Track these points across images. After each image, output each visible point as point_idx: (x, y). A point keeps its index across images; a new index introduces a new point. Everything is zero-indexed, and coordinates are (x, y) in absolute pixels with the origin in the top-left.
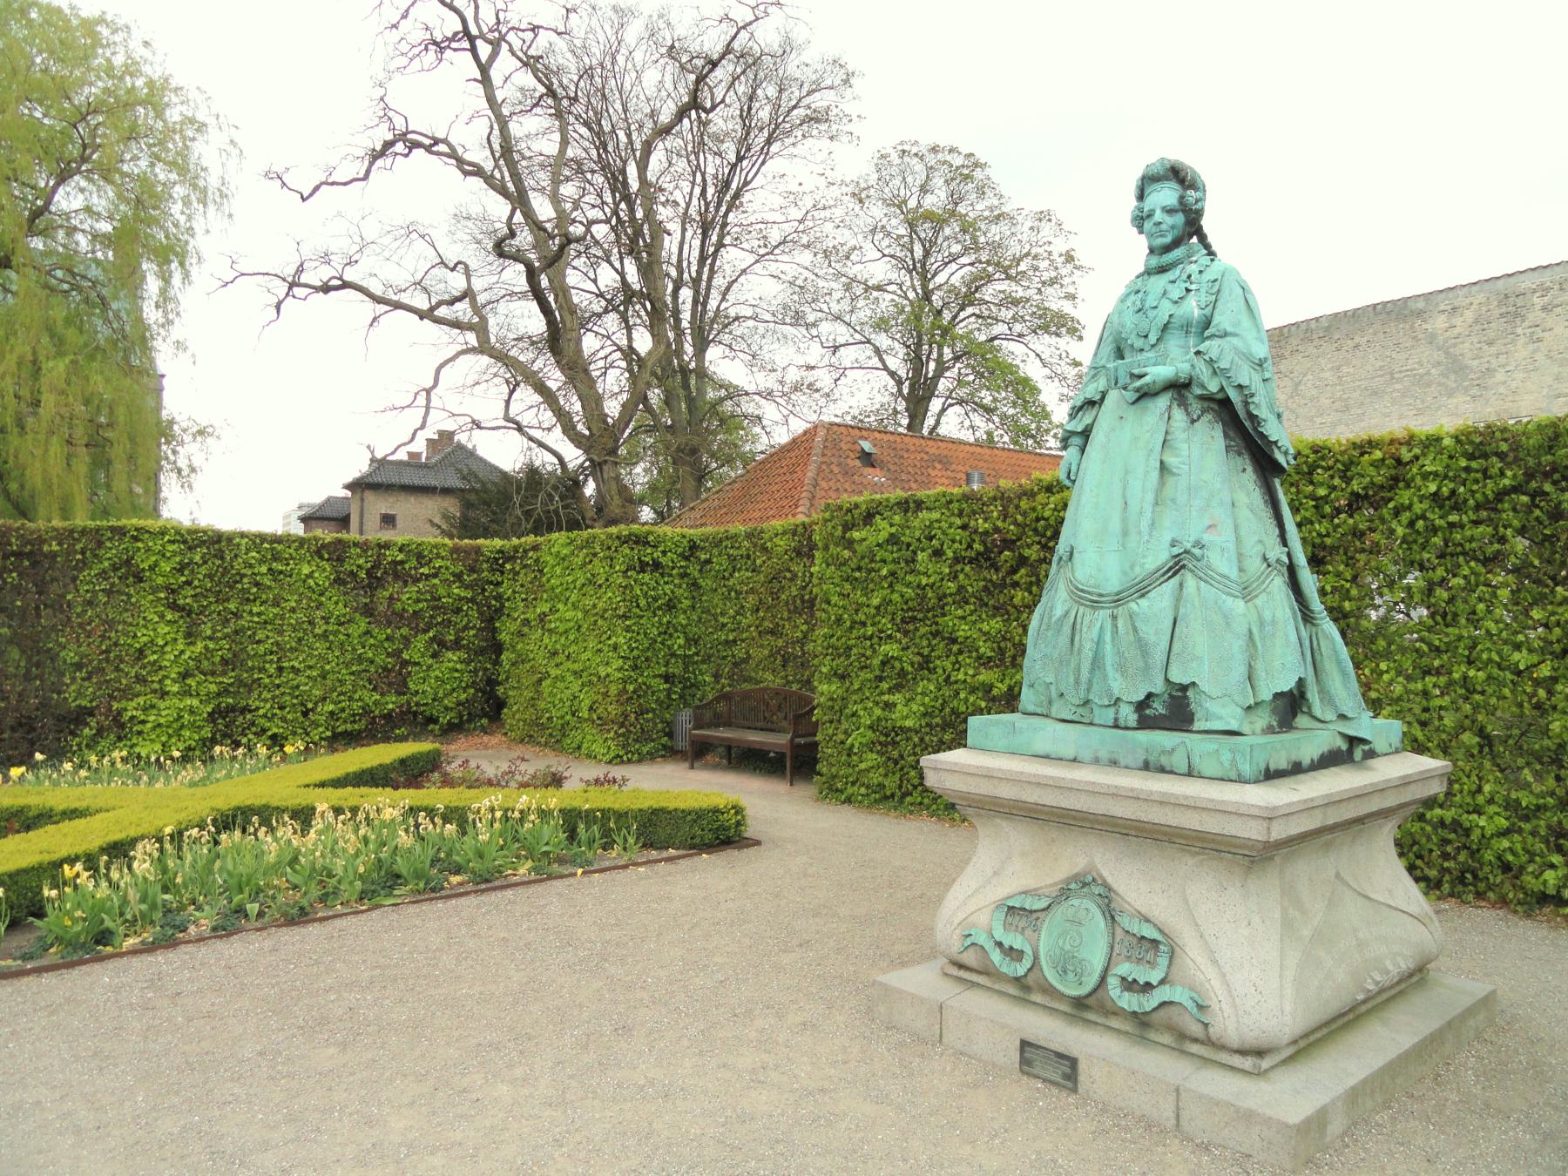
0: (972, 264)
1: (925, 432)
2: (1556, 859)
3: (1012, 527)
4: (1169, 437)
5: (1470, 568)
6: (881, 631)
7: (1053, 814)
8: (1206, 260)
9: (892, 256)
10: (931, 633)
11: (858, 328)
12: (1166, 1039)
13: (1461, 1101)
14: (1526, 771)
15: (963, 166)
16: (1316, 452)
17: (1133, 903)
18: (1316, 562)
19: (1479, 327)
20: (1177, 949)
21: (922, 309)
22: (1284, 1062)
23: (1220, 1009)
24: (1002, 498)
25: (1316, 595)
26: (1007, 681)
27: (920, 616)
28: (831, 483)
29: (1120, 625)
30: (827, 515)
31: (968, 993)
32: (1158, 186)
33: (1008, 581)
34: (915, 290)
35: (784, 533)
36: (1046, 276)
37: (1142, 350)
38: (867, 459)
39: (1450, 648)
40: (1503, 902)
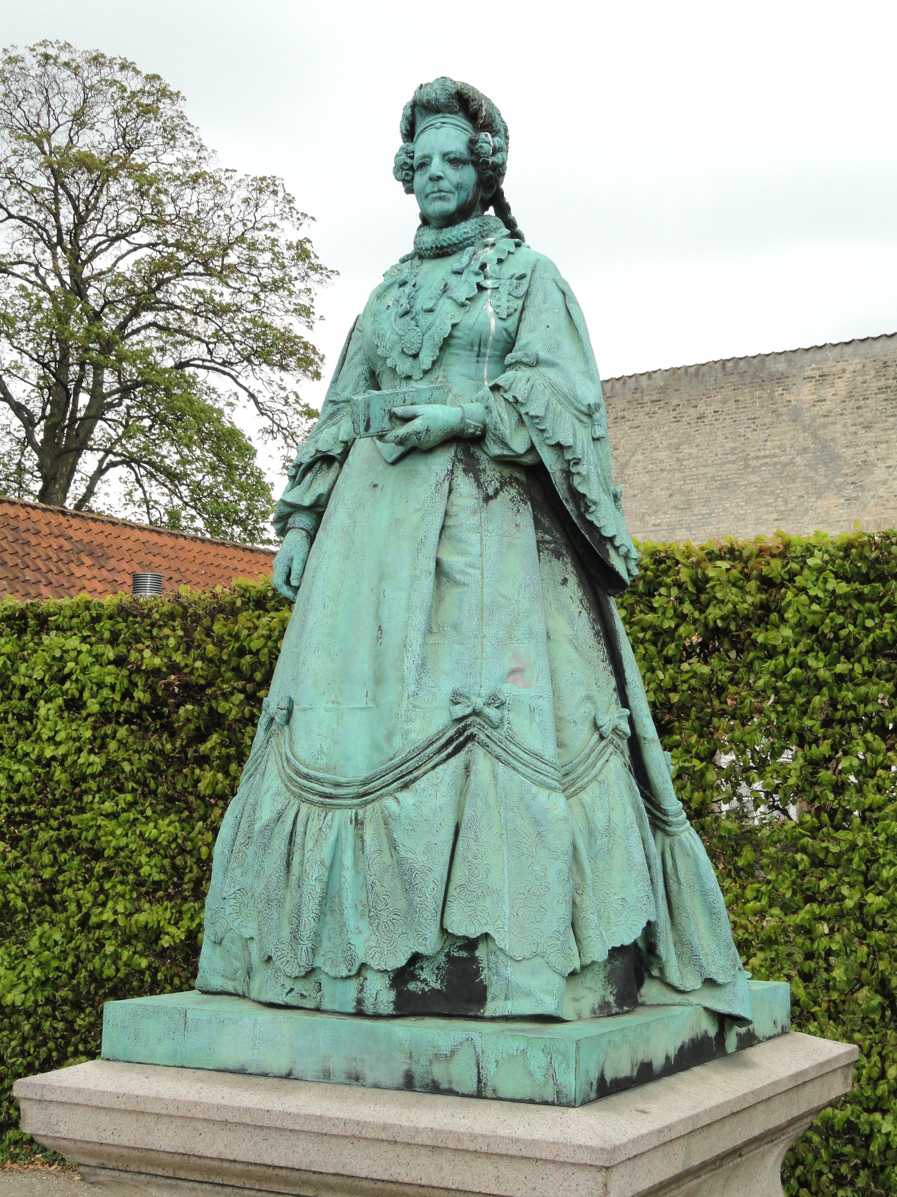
0: (152, 246)
1: (70, 504)
3: (198, 664)
4: (449, 522)
7: (247, 1175)
8: (510, 243)
9: (22, 219)
10: (59, 841)
15: (142, 91)
19: (852, 404)
24: (184, 616)
25: (670, 786)
26: (185, 923)
27: (41, 812)
29: (368, 838)
32: (437, 119)
33: (190, 753)
36: (267, 276)
37: (409, 378)
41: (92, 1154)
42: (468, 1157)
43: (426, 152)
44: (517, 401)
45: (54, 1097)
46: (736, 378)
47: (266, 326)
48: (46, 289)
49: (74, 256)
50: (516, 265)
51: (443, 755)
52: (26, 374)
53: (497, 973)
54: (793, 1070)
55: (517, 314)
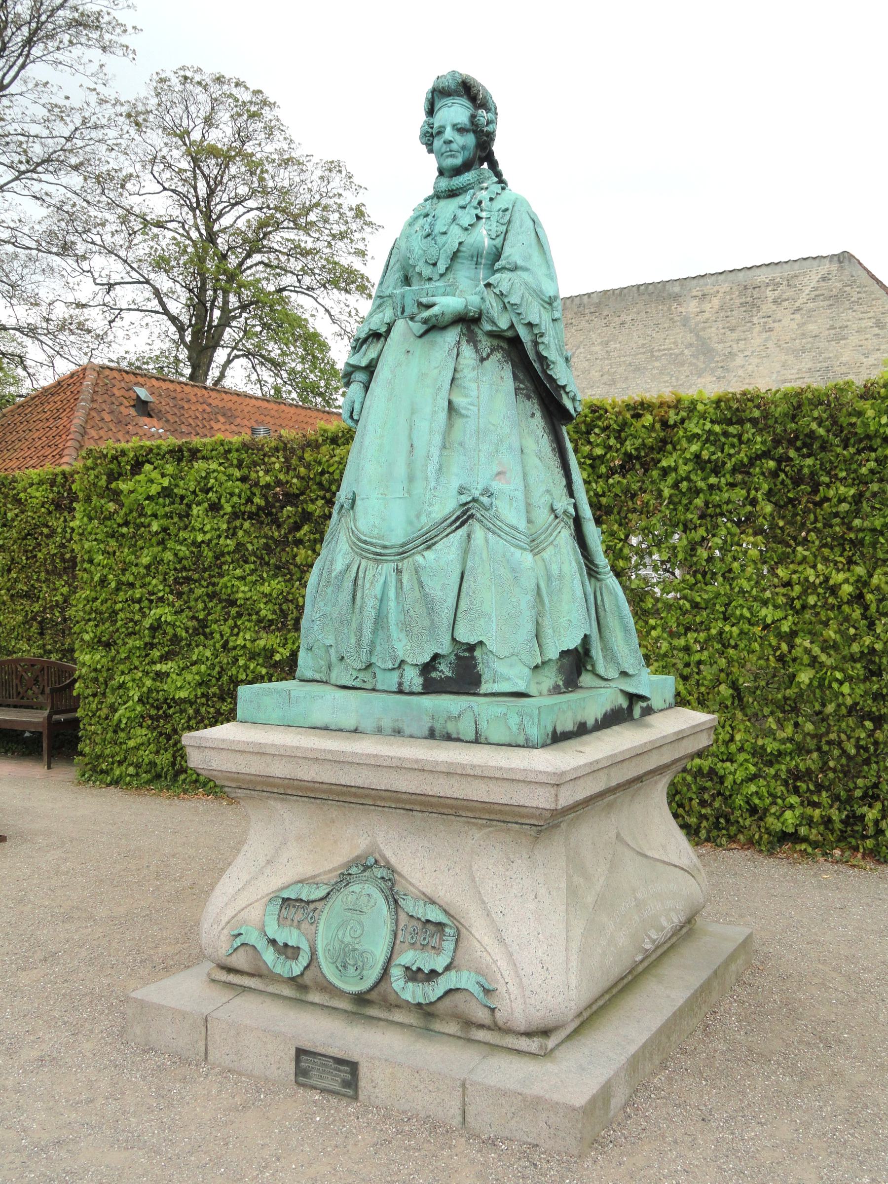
1: (209, 383)
2: (794, 799)
3: (295, 480)
4: (457, 376)
5: (727, 528)
6: (152, 593)
7: (331, 792)
9: (174, 191)
10: (208, 595)
11: (135, 266)
12: (452, 1028)
13: (728, 1050)
14: (771, 719)
15: (251, 102)
16: (593, 412)
17: (417, 884)
18: (601, 513)
19: (723, 314)
20: (463, 931)
21: (205, 251)
22: (569, 1037)
23: (507, 991)
24: (285, 449)
26: (289, 646)
28: (102, 433)
29: (405, 581)
30: (89, 462)
31: (238, 1001)
32: (449, 101)
34: (198, 230)
35: (41, 483)
36: (336, 229)
37: (430, 279)
38: (143, 407)
39: (709, 605)
40: (751, 843)
41: (233, 780)
42: (469, 779)
43: (442, 124)
44: (502, 294)
45: (208, 745)
46: (645, 297)
47: (336, 263)
48: (190, 239)
49: (208, 216)
50: (502, 202)
51: (453, 527)
52: (178, 297)
53: (488, 667)
54: (676, 729)
55: (502, 236)
